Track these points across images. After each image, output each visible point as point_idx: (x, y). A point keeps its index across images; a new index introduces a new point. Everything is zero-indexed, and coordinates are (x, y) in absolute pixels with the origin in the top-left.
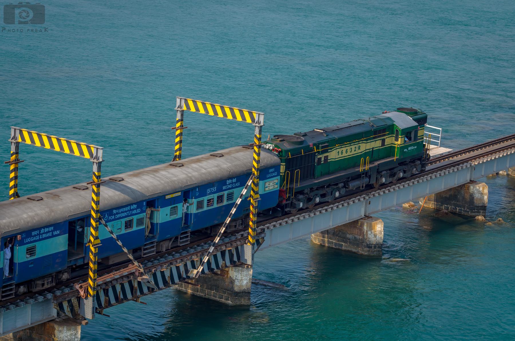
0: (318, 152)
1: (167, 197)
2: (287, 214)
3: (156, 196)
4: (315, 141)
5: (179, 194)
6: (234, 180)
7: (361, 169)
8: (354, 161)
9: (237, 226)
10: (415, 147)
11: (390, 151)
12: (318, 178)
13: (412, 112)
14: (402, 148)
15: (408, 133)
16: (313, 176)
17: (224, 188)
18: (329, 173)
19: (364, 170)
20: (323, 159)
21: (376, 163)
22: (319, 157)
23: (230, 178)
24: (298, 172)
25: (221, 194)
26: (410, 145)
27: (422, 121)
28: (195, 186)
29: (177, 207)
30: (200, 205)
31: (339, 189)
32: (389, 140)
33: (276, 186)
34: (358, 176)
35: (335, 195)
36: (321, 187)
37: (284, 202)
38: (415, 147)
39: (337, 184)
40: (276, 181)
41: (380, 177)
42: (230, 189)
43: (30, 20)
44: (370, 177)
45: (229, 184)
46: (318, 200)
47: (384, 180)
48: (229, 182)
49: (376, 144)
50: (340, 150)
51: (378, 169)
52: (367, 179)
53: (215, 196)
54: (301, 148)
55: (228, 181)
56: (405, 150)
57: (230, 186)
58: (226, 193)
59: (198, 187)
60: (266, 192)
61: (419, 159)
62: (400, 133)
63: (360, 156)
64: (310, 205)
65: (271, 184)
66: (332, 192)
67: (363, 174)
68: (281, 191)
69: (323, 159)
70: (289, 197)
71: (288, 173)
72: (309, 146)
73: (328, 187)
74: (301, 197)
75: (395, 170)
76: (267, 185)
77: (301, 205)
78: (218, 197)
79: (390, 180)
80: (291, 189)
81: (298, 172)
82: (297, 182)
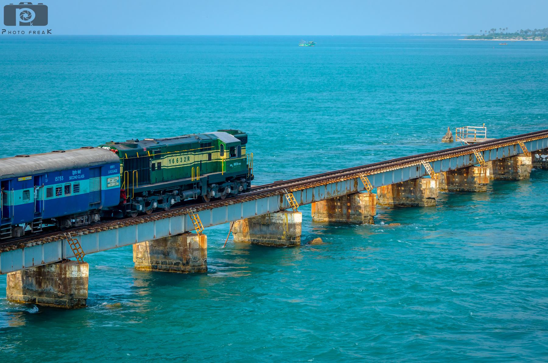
0: (152, 157)
1: (20, 179)
2: (127, 216)
3: (9, 177)
4: (148, 146)
5: (30, 178)
6: (79, 172)
7: (192, 179)
8: (184, 171)
9: (84, 221)
10: (240, 164)
11: (217, 166)
12: (153, 184)
13: (234, 133)
14: (228, 163)
15: (231, 148)
16: (149, 181)
17: (70, 178)
18: (163, 181)
19: (196, 179)
20: (156, 166)
21: (206, 175)
22: (153, 162)
23: (76, 168)
24: (135, 172)
25: (67, 184)
26: (235, 161)
27: (244, 140)
28: (44, 172)
29: (28, 191)
30: (49, 192)
31: (173, 197)
32: (216, 156)
33: (118, 184)
34: (190, 186)
35: (171, 202)
36: (157, 192)
37: (125, 203)
38: (240, 164)
39: (171, 191)
40: (117, 178)
41: (209, 190)
42: (75, 180)
43: (32, 22)
44: (201, 188)
45: (75, 175)
46: (155, 205)
47: (214, 193)
48: (74, 172)
49: (203, 157)
50: (171, 158)
51: (208, 181)
52: (199, 191)
53: (63, 185)
54: (136, 151)
55: (73, 172)
56: (231, 165)
57: (76, 177)
58: (73, 183)
59: (47, 173)
60: (108, 189)
61: (245, 177)
62: (225, 147)
63: (191, 167)
64: (148, 209)
65: (113, 181)
66: (168, 199)
67: (195, 184)
68: (123, 193)
69: (156, 166)
70: (129, 198)
71: (126, 173)
72: (143, 150)
73: (163, 193)
74: (140, 199)
75: (224, 185)
76: (109, 180)
77: (141, 208)
78: (66, 187)
79: (219, 195)
80: (131, 190)
81: (135, 172)
82: (135, 185)
